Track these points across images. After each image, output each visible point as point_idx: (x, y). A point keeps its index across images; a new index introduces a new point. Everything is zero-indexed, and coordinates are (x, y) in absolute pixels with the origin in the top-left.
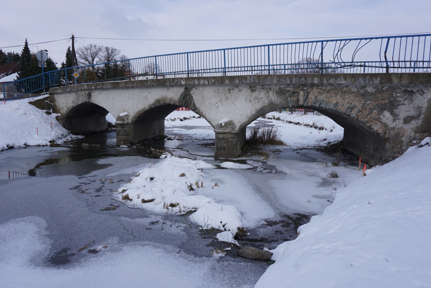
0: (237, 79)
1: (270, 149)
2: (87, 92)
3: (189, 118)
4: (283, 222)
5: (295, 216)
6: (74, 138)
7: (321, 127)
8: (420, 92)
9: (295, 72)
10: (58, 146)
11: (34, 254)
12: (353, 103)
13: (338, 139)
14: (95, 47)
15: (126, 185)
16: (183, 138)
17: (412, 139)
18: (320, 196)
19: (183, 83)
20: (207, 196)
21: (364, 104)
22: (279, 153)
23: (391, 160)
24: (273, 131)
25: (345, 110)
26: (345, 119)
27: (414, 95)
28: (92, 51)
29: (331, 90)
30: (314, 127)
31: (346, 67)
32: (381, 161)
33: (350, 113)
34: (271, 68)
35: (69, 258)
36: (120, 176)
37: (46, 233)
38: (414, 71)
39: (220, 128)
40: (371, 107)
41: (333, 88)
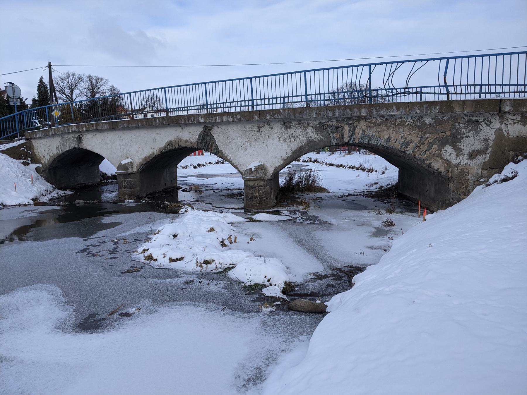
2: (77, 136)
3: (205, 164)
4: (333, 275)
5: (347, 269)
7: (370, 169)
8: (486, 122)
10: (44, 204)
12: (409, 138)
13: (392, 182)
14: (74, 76)
15: (144, 244)
16: (202, 188)
17: (479, 178)
18: (374, 247)
19: (202, 120)
21: (421, 138)
22: (321, 201)
23: (456, 203)
24: (312, 176)
25: (400, 146)
26: (400, 157)
27: (480, 126)
28: (70, 81)
29: (382, 123)
30: (361, 169)
31: (399, 95)
32: (444, 204)
33: (405, 149)
35: (100, 323)
36: (134, 235)
37: (64, 300)
38: (480, 97)
39: (250, 174)
40: (430, 141)
41: (384, 120)
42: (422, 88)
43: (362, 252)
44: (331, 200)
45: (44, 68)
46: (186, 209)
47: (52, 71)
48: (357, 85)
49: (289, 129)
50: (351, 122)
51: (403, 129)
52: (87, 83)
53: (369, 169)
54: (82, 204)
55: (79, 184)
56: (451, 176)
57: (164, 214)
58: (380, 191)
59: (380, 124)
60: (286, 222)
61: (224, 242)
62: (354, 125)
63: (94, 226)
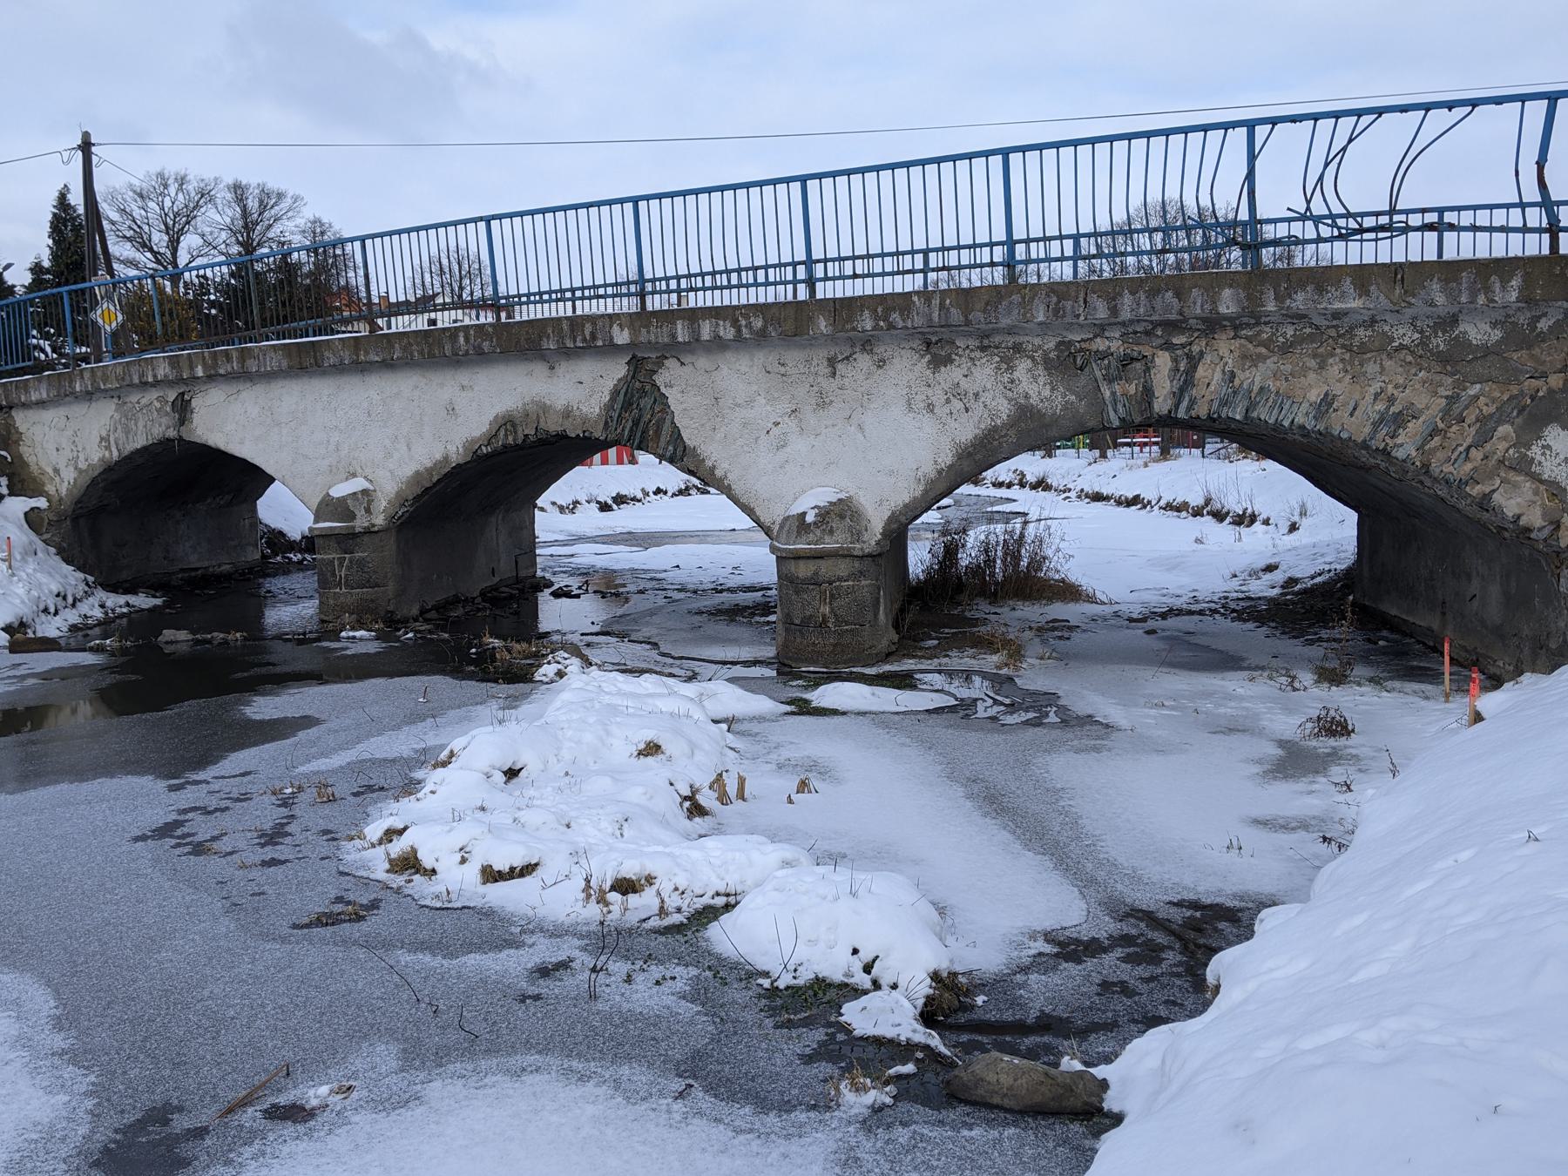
2: (172, 395)
3: (640, 495)
4: (1126, 940)
5: (1178, 915)
6: (113, 610)
7: (1244, 513)
9: (1105, 267)
10: (48, 645)
11: (20, 1139)
14: (182, 184)
15: (393, 806)
16: (624, 586)
18: (1281, 821)
19: (622, 337)
20: (773, 837)
21: (1452, 400)
24: (1029, 538)
25: (1367, 430)
26: (1367, 469)
28: (168, 203)
29: (1298, 341)
30: (1208, 513)
33: (1388, 440)
35: (185, 1149)
37: (59, 1041)
39: (799, 533)
40: (1485, 408)
41: (1308, 330)
42: (1446, 214)
43: (1235, 843)
44: (1105, 631)
45: (66, 155)
46: (560, 666)
47: (94, 163)
48: (1191, 209)
49: (945, 366)
51: (1381, 364)
52: (226, 209)
53: (1241, 513)
54: (184, 648)
55: (182, 570)
57: (478, 684)
58: (1288, 597)
59: (1291, 346)
60: (935, 716)
61: (697, 797)
63: (216, 734)
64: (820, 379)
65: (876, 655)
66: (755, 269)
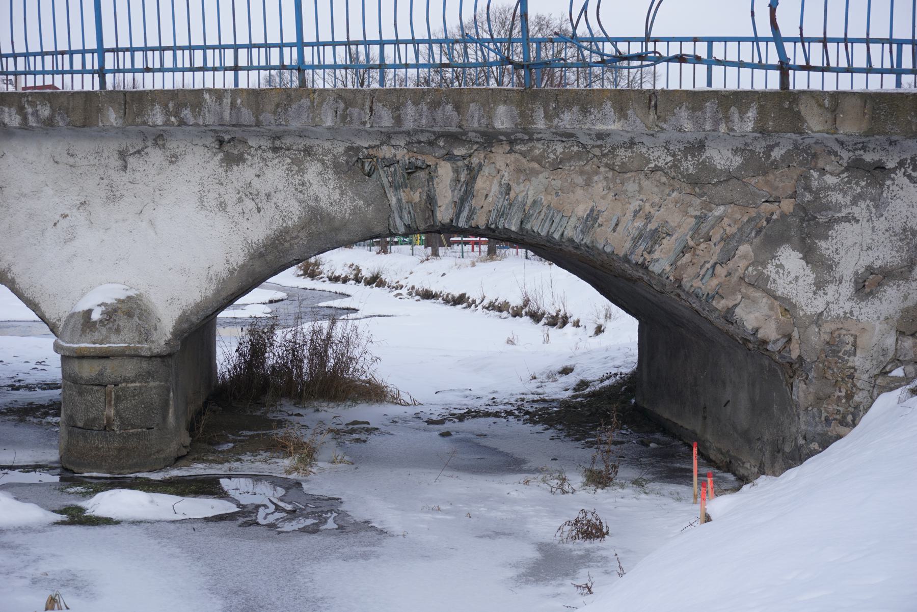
0: (157, 108)
1: (321, 422)
7: (557, 315)
8: (909, 171)
12: (659, 215)
21: (701, 219)
22: (363, 437)
25: (628, 245)
27: (888, 182)
30: (527, 314)
32: (780, 454)
33: (646, 255)
34: (308, 59)
38: (899, 84)
39: (83, 331)
40: (728, 229)
41: (575, 149)
49: (238, 165)
50: (459, 151)
53: (554, 314)
56: (799, 356)
58: (579, 400)
59: (560, 163)
62: (470, 161)
64: (111, 172)
65: (164, 459)
66: (132, 50)
